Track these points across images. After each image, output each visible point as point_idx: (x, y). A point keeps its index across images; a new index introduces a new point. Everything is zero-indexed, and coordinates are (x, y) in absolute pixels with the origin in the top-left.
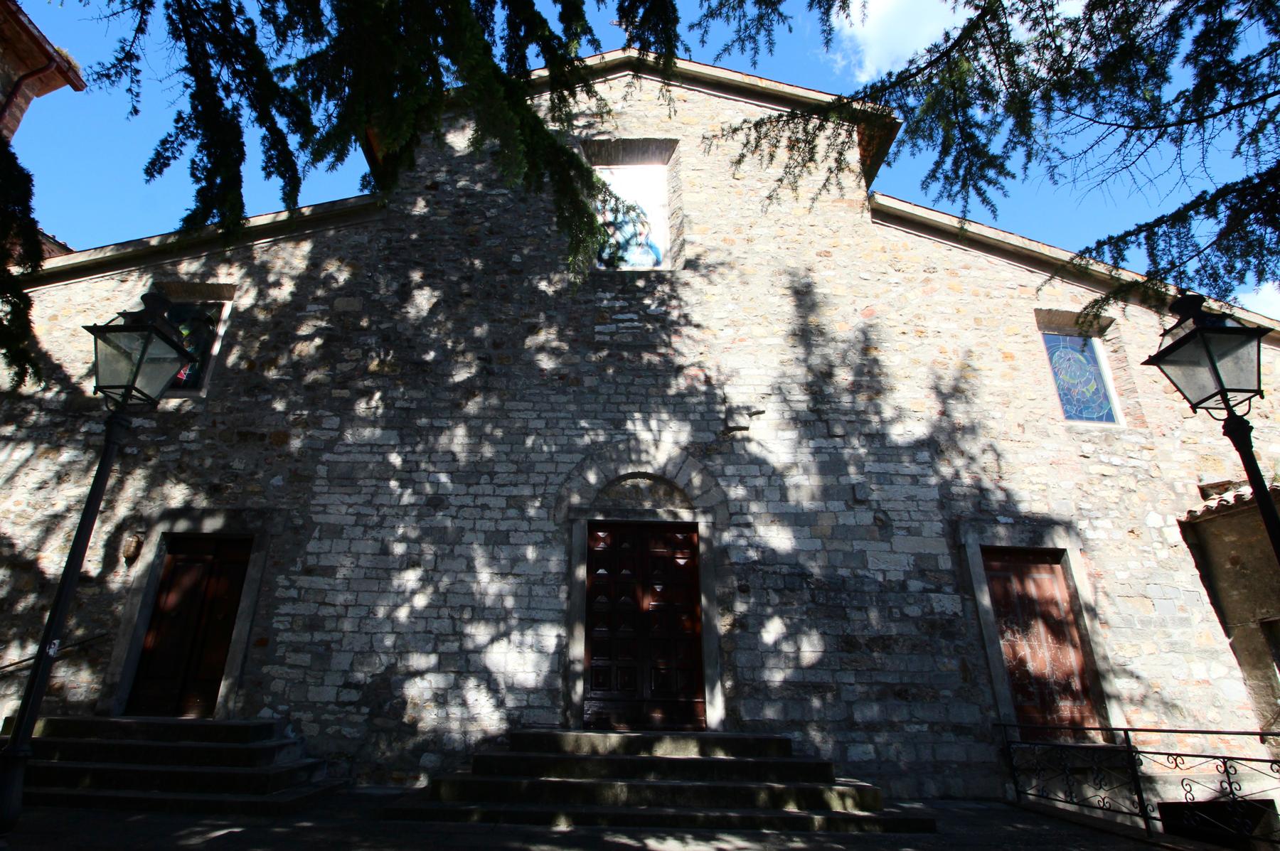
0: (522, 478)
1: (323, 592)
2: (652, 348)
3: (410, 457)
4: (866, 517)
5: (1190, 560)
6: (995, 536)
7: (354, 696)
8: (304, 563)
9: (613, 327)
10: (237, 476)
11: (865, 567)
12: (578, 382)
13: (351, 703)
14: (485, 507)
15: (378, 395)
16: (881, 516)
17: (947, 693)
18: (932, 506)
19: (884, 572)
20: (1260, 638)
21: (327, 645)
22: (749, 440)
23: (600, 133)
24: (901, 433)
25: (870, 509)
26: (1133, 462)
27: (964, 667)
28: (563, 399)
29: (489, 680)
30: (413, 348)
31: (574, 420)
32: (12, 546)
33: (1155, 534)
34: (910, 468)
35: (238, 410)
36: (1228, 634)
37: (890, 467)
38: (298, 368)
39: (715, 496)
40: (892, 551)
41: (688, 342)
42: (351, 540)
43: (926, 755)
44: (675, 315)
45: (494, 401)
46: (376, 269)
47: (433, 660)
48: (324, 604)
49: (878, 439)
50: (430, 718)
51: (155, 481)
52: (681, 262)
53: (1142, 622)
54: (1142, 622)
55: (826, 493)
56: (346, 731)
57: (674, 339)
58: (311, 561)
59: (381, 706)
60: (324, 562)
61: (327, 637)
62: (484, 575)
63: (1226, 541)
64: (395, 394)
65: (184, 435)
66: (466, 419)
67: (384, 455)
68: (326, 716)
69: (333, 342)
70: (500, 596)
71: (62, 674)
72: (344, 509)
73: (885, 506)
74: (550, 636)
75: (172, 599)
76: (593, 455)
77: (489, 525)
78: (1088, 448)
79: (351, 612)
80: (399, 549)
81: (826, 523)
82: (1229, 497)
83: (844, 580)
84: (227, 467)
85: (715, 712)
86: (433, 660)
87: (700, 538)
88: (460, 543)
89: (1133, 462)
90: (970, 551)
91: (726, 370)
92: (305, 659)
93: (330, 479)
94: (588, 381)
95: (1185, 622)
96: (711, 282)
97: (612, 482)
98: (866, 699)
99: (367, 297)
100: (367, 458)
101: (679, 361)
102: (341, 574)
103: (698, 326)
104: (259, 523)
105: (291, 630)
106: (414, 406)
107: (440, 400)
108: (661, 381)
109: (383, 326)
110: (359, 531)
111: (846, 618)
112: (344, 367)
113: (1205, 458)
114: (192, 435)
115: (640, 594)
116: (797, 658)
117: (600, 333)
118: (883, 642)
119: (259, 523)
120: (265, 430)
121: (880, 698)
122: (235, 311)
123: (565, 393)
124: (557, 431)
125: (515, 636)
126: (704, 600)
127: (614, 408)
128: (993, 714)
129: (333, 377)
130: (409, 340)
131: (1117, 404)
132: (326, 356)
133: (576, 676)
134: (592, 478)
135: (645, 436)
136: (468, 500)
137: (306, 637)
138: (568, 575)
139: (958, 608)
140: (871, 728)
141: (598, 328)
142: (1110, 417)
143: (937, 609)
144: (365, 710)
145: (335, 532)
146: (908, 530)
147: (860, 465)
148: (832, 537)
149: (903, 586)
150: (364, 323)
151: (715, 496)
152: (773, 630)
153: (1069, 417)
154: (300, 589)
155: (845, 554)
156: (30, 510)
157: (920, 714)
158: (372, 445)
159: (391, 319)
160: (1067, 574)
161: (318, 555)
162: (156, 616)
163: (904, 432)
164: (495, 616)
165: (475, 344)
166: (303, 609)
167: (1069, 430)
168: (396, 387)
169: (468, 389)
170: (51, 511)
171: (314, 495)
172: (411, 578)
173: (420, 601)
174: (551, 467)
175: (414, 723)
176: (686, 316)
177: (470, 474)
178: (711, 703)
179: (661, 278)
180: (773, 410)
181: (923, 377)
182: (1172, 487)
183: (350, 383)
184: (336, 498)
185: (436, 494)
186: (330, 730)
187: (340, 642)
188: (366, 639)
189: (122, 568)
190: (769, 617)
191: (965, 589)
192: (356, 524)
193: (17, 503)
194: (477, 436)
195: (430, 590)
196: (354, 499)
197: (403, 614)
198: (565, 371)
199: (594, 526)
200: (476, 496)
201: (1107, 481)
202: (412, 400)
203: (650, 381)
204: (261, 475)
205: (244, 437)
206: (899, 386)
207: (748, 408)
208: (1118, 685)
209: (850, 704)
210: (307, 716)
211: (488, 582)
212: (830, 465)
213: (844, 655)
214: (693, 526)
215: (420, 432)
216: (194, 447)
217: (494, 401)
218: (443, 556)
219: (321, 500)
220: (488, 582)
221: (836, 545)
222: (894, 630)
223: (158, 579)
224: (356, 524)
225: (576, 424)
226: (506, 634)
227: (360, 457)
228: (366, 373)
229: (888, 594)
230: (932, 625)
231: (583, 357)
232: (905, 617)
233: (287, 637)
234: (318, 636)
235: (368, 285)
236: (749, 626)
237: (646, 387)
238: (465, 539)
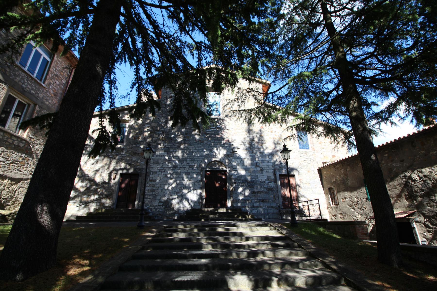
0: (192, 162)
1: (153, 184)
2: (218, 135)
3: (170, 158)
4: (258, 169)
5: (319, 176)
6: (282, 172)
7: (161, 204)
8: (150, 179)
9: (210, 130)
10: (134, 162)
11: (258, 179)
12: (203, 142)
13: (161, 205)
14: (185, 168)
15: (162, 144)
16: (261, 169)
17: (271, 201)
18: (271, 167)
19: (261, 179)
20: (328, 191)
21: (156, 195)
22: (237, 154)
23: (146, 7)
24: (266, 152)
25: (259, 167)
26: (310, 158)
27: (274, 197)
28: (200, 145)
29: (187, 200)
30: (169, 134)
31: (203, 149)
32: (89, 177)
33: (313, 172)
34: (268, 159)
35: (133, 148)
36: (324, 190)
37: (264, 159)
38: (145, 138)
39: (230, 165)
40: (263, 175)
41: (226, 133)
42: (159, 174)
43: (266, 212)
44: (223, 127)
45: (186, 145)
46: (160, 117)
47: (176, 196)
48: (154, 187)
49: (262, 153)
50: (176, 207)
51: (117, 163)
52: (224, 115)
53: (308, 188)
54: (308, 188)
55: (252, 164)
56: (160, 210)
57: (223, 132)
58: (151, 179)
59: (167, 206)
60: (154, 179)
61: (156, 193)
62: (186, 180)
63: (324, 173)
64: (166, 144)
65: (122, 153)
66: (181, 149)
67: (164, 157)
68: (156, 208)
69: (153, 132)
70: (189, 185)
71: (104, 201)
72: (157, 168)
73: (262, 167)
74: (199, 191)
75: (123, 186)
76: (207, 157)
77: (186, 171)
78: (302, 155)
79: (160, 188)
80: (169, 176)
81: (251, 170)
82: (326, 164)
83: (253, 181)
84: (132, 160)
85: (229, 204)
86: (176, 196)
87: (227, 173)
88: (180, 175)
89: (310, 158)
90: (277, 175)
91: (233, 139)
92: (151, 197)
93: (154, 162)
94: (205, 142)
95: (316, 188)
96: (231, 120)
97: (210, 163)
98: (256, 202)
99: (158, 123)
100: (161, 158)
101: (224, 137)
102: (158, 181)
103: (227, 129)
104: (140, 171)
105: (148, 192)
106: (170, 147)
107: (175, 146)
108: (220, 141)
109: (162, 130)
110: (160, 173)
111: (253, 188)
112: (154, 139)
113: (325, 157)
114: (124, 153)
115: (215, 183)
116: (245, 194)
117: (208, 131)
118: (260, 192)
119: (140, 171)
120: (139, 152)
121: (259, 202)
122: (129, 126)
123: (201, 144)
124: (199, 152)
125: (192, 191)
126: (228, 184)
127: (210, 147)
128: (278, 204)
129: (152, 141)
130: (168, 133)
131: (310, 146)
132: (150, 136)
133: (204, 199)
134: (206, 161)
135: (217, 152)
136: (182, 166)
137: (151, 193)
138: (202, 180)
139: (274, 186)
140: (257, 207)
141: (207, 130)
142: (308, 148)
143: (270, 186)
144: (164, 206)
145: (155, 173)
146: (266, 171)
147: (258, 158)
148: (252, 173)
149: (265, 182)
150: (213, 144)
151: (230, 165)
152: (240, 190)
153: (300, 148)
154: (149, 184)
155: (254, 176)
156: (91, 169)
157: (266, 205)
158: (162, 155)
159: (164, 128)
160: (295, 180)
161: (152, 177)
162: (120, 189)
163: (268, 151)
164: (188, 188)
165: (182, 133)
166: (150, 188)
167: (299, 151)
168: (166, 143)
169: (181, 143)
170: (95, 169)
171: (150, 166)
172: (171, 181)
173: (174, 185)
174: (198, 160)
175: (173, 208)
176: (225, 127)
177: (182, 161)
178: (229, 203)
179: (220, 119)
180: (242, 147)
181: (272, 140)
182: (317, 163)
183: (156, 142)
184: (155, 166)
185: (175, 165)
186: (157, 210)
187: (158, 194)
188: (163, 193)
189: (113, 181)
190: (240, 187)
191: (276, 182)
192: (160, 171)
193: (88, 168)
194: (183, 152)
195: (175, 183)
196: (158, 166)
197: (170, 188)
198: (201, 139)
199: (207, 171)
200: (183, 165)
201: (305, 162)
202: (169, 146)
203: (218, 142)
204: (139, 161)
205: (135, 154)
206: (267, 143)
207: (237, 147)
208: (302, 199)
209: (253, 203)
210: (153, 208)
211: (186, 182)
212: (253, 159)
213: (253, 195)
214: (226, 171)
215: (171, 152)
216: (124, 156)
217: (186, 145)
218: (177, 177)
219: (152, 167)
220: (186, 182)
221: (253, 174)
222: (262, 189)
223: (120, 183)
224: (160, 171)
225: (203, 150)
226: (190, 191)
227: (159, 158)
228: (159, 139)
229: (262, 183)
230: (269, 189)
231: (204, 137)
232: (264, 187)
233: (147, 193)
234: (154, 193)
235: (158, 120)
236: (236, 189)
237: (217, 143)
238: (181, 174)
